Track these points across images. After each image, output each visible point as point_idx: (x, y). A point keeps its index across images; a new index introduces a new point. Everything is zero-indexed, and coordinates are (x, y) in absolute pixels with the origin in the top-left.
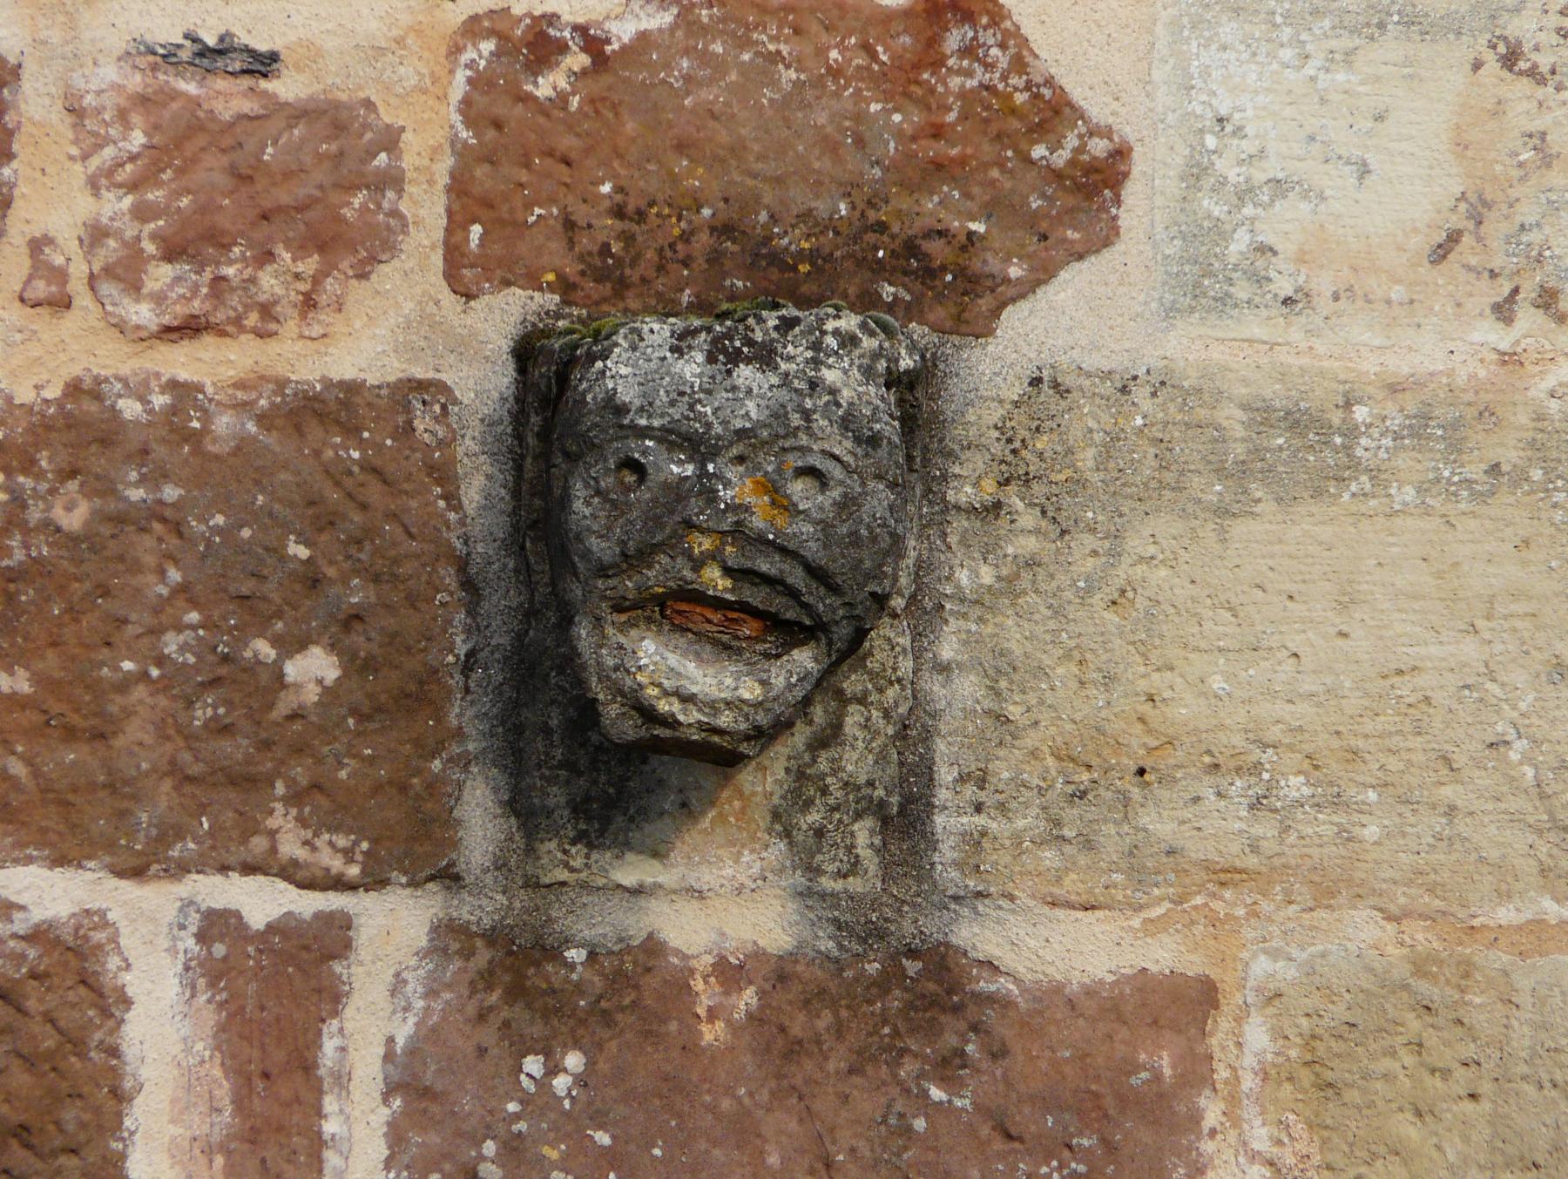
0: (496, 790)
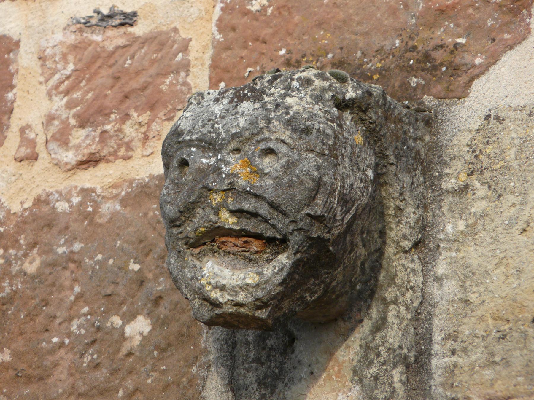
0: (222, 378)
